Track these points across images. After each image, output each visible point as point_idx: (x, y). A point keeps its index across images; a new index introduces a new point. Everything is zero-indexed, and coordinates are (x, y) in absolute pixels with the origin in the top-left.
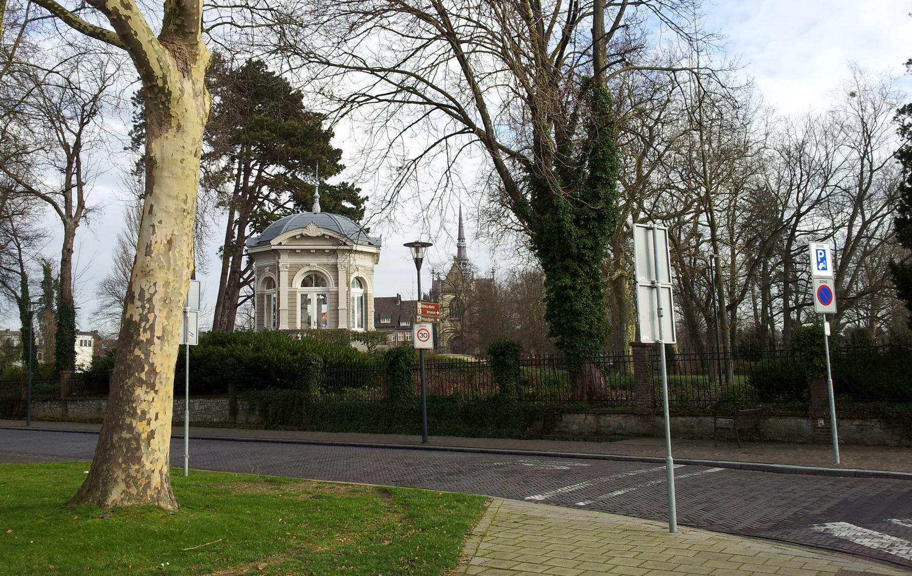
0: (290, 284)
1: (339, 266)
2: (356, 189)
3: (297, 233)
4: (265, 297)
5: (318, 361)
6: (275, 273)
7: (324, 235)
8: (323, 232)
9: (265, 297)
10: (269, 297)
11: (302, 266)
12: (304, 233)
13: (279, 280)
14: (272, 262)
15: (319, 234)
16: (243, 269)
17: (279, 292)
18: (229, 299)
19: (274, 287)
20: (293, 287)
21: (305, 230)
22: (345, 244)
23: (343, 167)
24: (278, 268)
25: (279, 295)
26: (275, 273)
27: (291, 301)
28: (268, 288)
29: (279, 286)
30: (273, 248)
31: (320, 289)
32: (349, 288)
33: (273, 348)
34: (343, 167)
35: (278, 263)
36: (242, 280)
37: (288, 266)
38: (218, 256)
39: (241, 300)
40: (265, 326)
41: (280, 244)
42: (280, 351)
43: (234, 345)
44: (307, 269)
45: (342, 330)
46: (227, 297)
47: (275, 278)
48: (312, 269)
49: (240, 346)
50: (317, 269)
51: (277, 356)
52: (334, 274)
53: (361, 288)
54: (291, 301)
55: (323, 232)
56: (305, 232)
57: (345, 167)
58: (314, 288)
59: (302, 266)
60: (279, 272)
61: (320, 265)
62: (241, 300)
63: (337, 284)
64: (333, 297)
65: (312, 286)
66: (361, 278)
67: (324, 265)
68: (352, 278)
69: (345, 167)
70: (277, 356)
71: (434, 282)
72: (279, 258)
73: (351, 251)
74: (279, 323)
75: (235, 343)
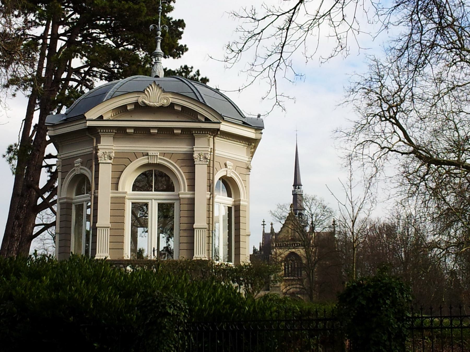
0: (116, 185)
1: (196, 155)
2: (202, 79)
3: (129, 100)
4: (73, 207)
5: (180, 309)
6: (90, 168)
7: (172, 105)
8: (172, 99)
9: (73, 207)
10: (80, 208)
11: (136, 155)
12: (140, 101)
13: (97, 178)
14: (86, 149)
15: (165, 102)
16: (41, 185)
17: (96, 198)
18: (19, 226)
19: (89, 189)
20: (120, 189)
21: (142, 95)
22: (207, 120)
23: (183, 49)
24: (97, 158)
25: (96, 203)
26: (90, 168)
27: (116, 207)
28: (79, 193)
29: (97, 188)
30: (89, 124)
31: (163, 196)
32: (212, 194)
33: (87, 283)
34: (183, 49)
35: (97, 150)
36: (40, 201)
37: (113, 155)
38: (5, 159)
39: (36, 230)
40: (72, 250)
41: (101, 118)
42: (100, 289)
43: (13, 278)
44: (143, 161)
45: (201, 263)
46: (17, 223)
47: (90, 175)
48: (151, 161)
49: (25, 280)
50: (159, 161)
51: (95, 298)
52: (187, 169)
53: (229, 195)
54: (116, 207)
55: (171, 100)
56: (142, 99)
57: (187, 50)
58: (153, 192)
59: (136, 155)
60: (97, 165)
61: (164, 154)
62: (36, 230)
63: (192, 187)
64: (185, 207)
65: (151, 191)
66: (231, 179)
67: (171, 155)
68: (217, 177)
69: (187, 50)
70: (95, 298)
71: (265, 235)
72: (98, 141)
73: (216, 132)
74: (94, 250)
75: (18, 275)
